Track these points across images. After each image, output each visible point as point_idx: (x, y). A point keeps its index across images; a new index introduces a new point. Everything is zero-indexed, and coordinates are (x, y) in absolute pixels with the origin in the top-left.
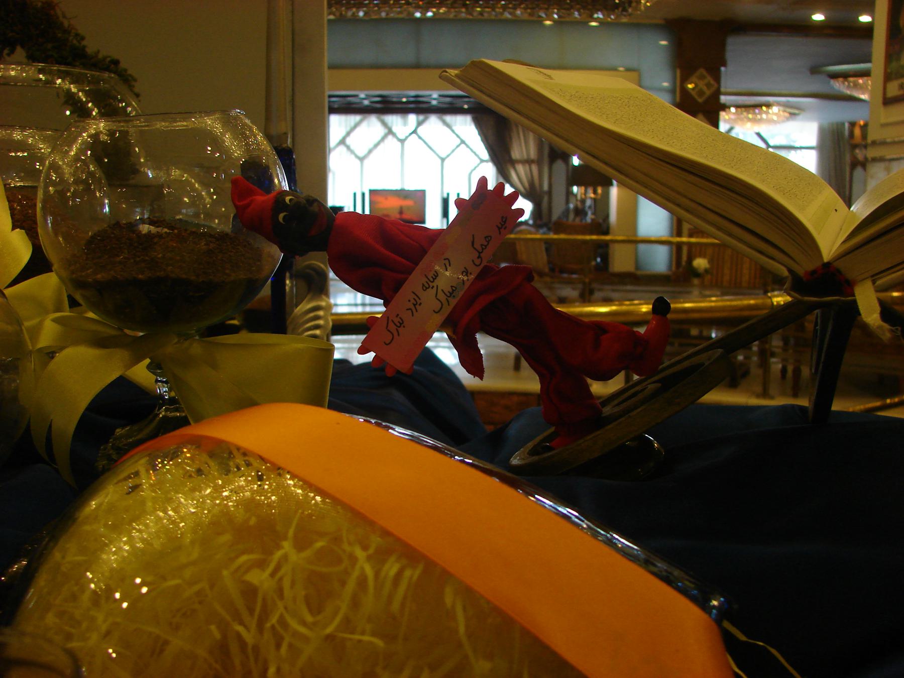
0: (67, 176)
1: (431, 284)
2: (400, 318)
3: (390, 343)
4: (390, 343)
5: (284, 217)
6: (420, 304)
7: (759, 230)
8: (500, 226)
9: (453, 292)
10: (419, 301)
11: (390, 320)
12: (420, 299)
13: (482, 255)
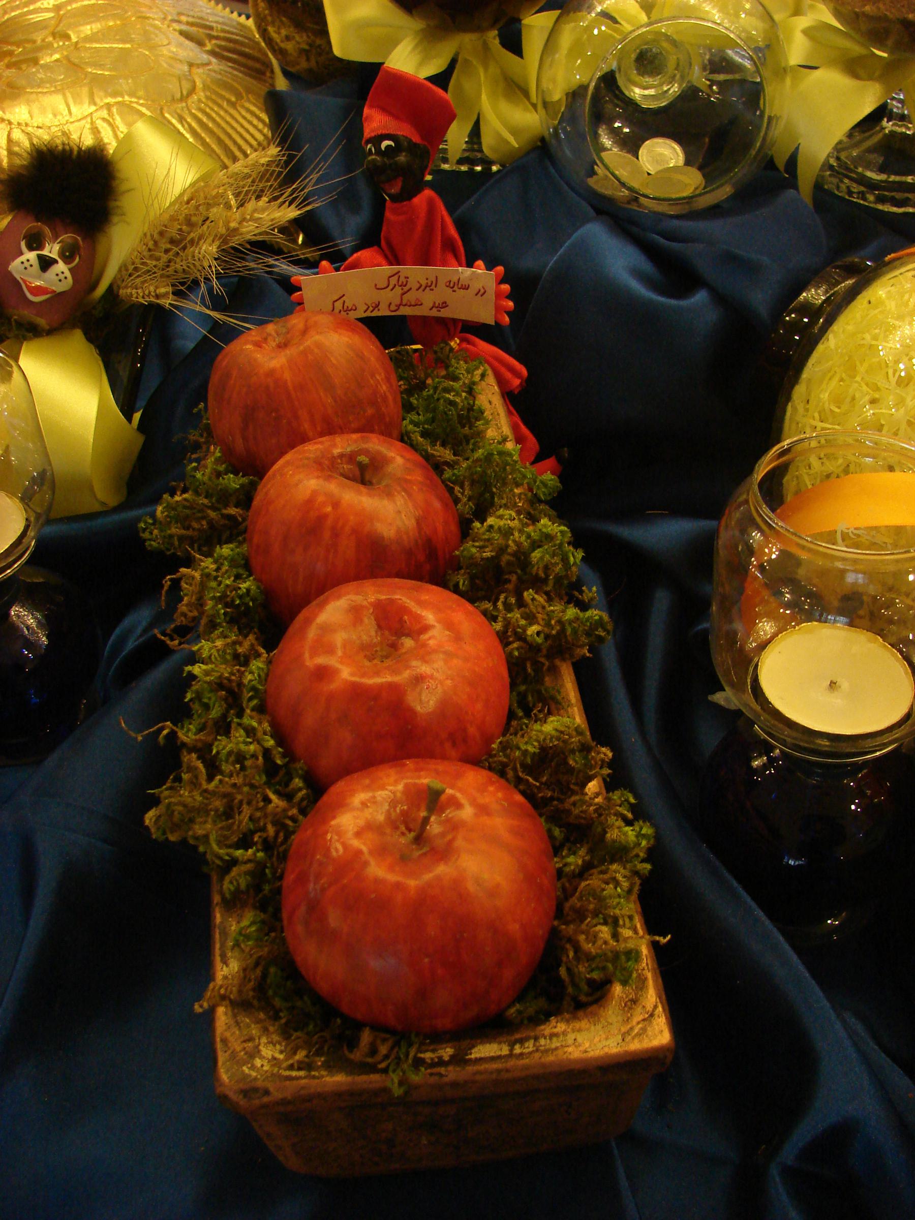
0: (354, 637)
1: (455, 288)
2: (407, 281)
3: (378, 289)
4: (378, 289)
5: (388, 147)
6: (432, 290)
7: (847, 554)
8: (437, 305)
9: (350, 310)
10: (433, 287)
11: (343, 299)
12: (436, 286)
13: (402, 307)
